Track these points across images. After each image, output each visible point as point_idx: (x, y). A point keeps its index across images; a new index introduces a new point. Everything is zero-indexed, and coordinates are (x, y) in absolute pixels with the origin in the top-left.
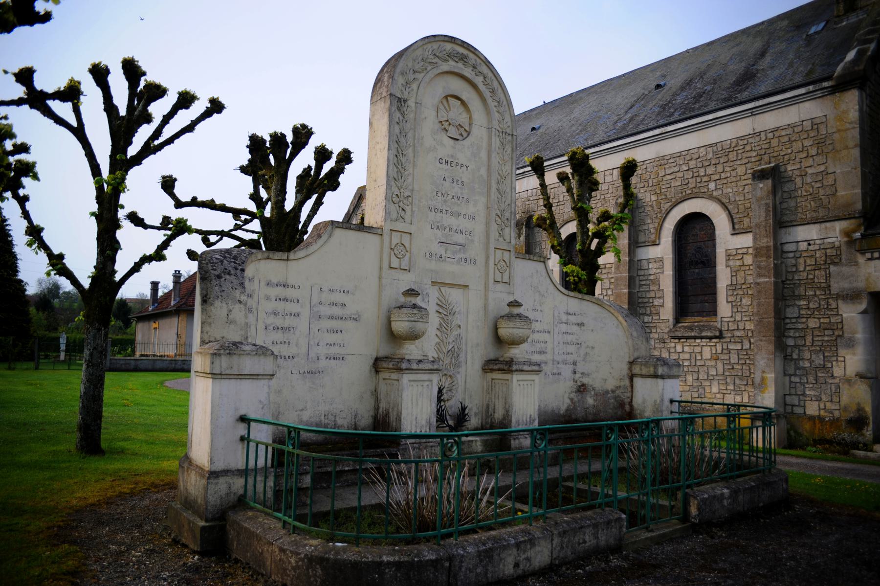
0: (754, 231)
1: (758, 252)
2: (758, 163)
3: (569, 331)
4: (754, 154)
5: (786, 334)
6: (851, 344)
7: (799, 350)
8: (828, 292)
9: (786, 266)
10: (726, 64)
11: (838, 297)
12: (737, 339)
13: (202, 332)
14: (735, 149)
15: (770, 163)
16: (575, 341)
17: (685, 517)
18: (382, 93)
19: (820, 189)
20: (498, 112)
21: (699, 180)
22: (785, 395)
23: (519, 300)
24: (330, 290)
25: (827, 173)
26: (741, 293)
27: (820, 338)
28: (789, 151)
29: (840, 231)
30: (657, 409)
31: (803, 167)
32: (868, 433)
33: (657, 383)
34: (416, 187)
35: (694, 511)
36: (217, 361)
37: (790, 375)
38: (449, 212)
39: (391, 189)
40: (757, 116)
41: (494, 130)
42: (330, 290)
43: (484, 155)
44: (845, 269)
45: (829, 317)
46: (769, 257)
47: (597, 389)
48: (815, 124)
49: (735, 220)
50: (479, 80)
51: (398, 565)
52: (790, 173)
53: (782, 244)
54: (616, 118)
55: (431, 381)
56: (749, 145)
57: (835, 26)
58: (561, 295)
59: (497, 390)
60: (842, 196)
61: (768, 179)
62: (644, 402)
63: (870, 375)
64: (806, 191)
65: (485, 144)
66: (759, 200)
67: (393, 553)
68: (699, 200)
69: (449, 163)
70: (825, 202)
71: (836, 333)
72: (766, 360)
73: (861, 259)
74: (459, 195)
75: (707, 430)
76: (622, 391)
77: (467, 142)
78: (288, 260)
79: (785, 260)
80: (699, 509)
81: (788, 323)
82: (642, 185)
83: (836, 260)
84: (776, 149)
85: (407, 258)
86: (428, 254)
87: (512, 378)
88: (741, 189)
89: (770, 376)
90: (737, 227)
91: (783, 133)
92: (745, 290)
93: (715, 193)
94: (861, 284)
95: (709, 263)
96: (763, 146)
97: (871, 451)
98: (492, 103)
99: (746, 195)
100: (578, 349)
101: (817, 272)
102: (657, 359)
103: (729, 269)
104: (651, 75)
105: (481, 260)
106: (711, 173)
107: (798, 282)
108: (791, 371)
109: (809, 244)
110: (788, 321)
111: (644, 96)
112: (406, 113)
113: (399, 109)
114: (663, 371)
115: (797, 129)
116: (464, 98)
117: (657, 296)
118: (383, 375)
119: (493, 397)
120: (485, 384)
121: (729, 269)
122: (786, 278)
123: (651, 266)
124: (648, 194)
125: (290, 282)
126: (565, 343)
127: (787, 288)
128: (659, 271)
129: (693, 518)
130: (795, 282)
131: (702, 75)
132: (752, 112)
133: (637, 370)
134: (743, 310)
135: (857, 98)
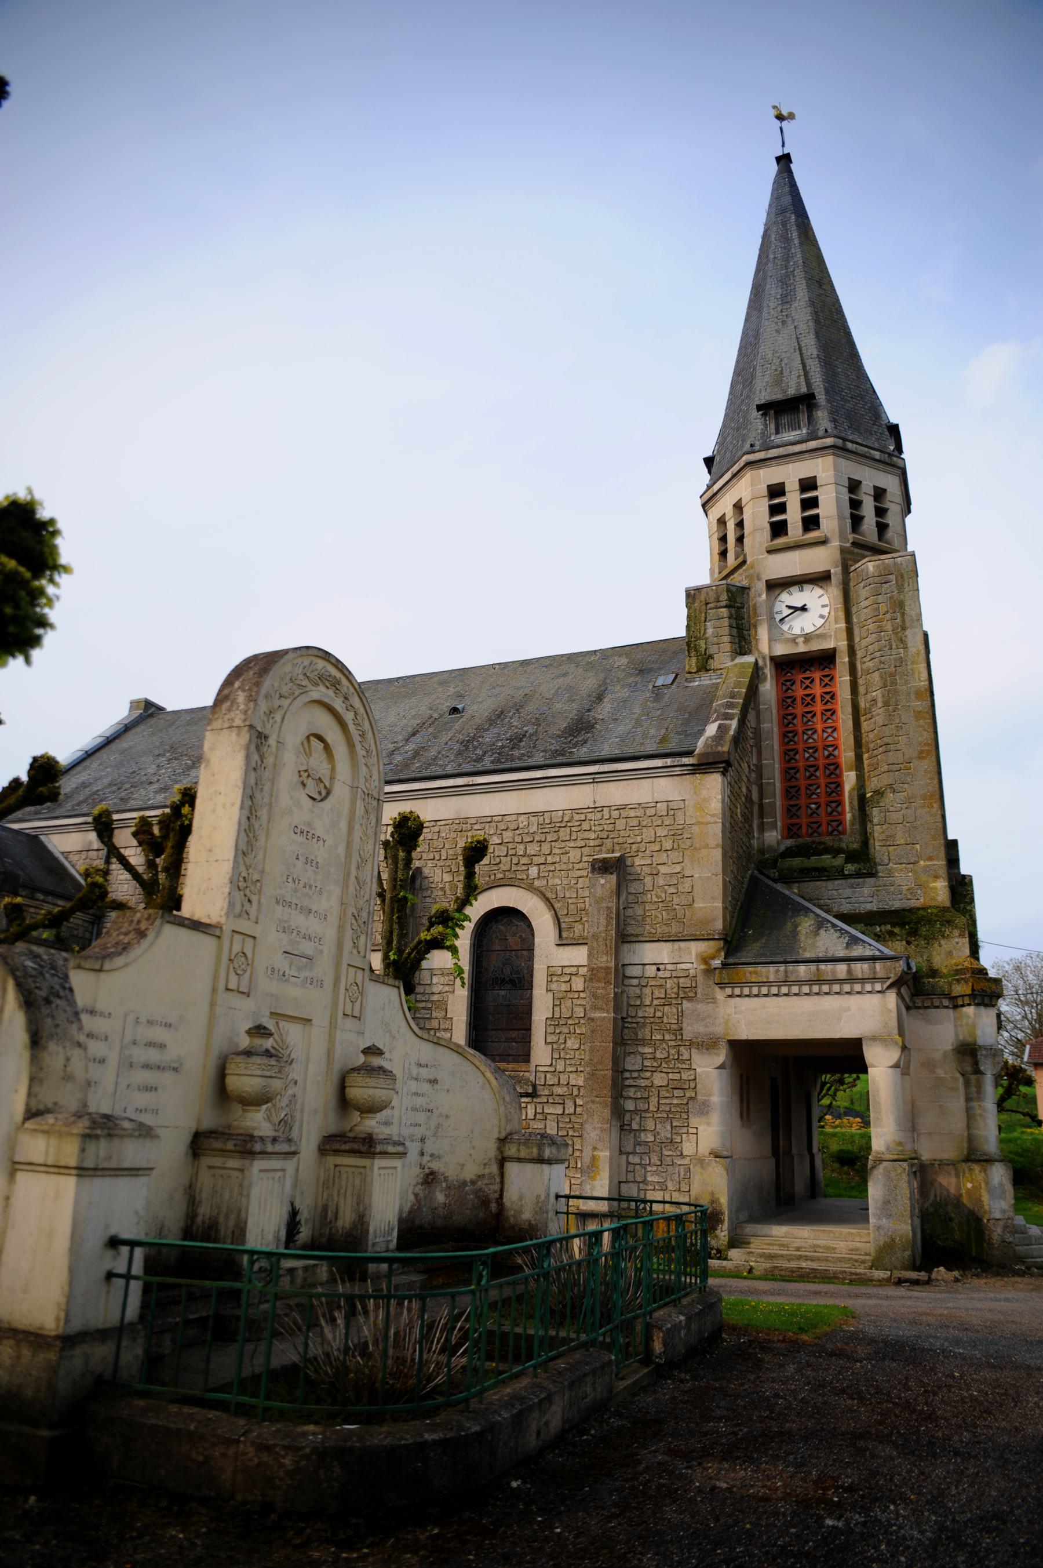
0: (589, 942)
1: (594, 974)
2: (597, 849)
3: (419, 1092)
4: (593, 836)
5: (624, 1093)
6: (704, 1110)
7: (641, 1117)
8: (679, 1037)
9: (628, 997)
10: (551, 699)
11: (692, 1044)
12: (557, 1098)
13: (29, 1095)
14: (569, 824)
15: (613, 852)
16: (425, 1106)
17: (647, 1359)
18: (233, 720)
19: (674, 896)
20: (366, 765)
21: (515, 860)
22: (620, 1182)
23: (381, 1046)
24: (148, 1022)
25: (684, 876)
26: (566, 1031)
27: (667, 1101)
28: (639, 839)
29: (697, 955)
30: (540, 1208)
31: (655, 863)
32: (723, 1234)
33: (542, 1170)
34: (267, 869)
35: (658, 1347)
36: (91, 1148)
37: (628, 1154)
38: (299, 906)
39: (238, 868)
40: (600, 785)
41: (359, 790)
42: (148, 1022)
43: (343, 825)
44: (701, 1007)
45: (679, 1072)
46: (608, 983)
47: (450, 1179)
48: (672, 810)
49: (563, 925)
50: (348, 717)
51: (443, 1443)
52: (639, 868)
53: (623, 965)
54: (391, 746)
55: (284, 1170)
56: (587, 821)
57: (686, 684)
58: (413, 1037)
59: (344, 1182)
60: (701, 909)
61: (611, 873)
62: (521, 1199)
63: (725, 1153)
64: (657, 897)
65: (346, 811)
66: (598, 901)
67: (432, 1428)
68: (515, 888)
69: (305, 833)
70: (680, 914)
71: (688, 1095)
72: (598, 1132)
73: (720, 995)
74: (312, 882)
75: (555, 1237)
76: (486, 1182)
77: (326, 805)
78: (100, 970)
79: (626, 989)
80: (665, 1344)
81: (627, 1078)
82: (431, 856)
83: (691, 994)
84: (622, 833)
85: (247, 975)
86: (269, 969)
87: (373, 1164)
88: (573, 882)
89: (604, 1155)
90: (564, 935)
91: (632, 813)
92: (572, 1027)
93: (537, 883)
94: (718, 1029)
95: (522, 982)
96: (605, 826)
97: (726, 1259)
98: (361, 752)
99: (580, 890)
100: (429, 1118)
101: (666, 1008)
102: (542, 1135)
103: (550, 995)
104: (440, 690)
105: (329, 983)
106: (533, 853)
107: (642, 1020)
108: (630, 1149)
109: (658, 969)
110: (627, 1075)
111: (431, 721)
112: (266, 756)
113: (258, 748)
114: (551, 1153)
115: (651, 812)
116: (329, 740)
117: (442, 1027)
118: (206, 1161)
119: (335, 1194)
120: (322, 1173)
121: (550, 995)
122: (627, 1014)
123: (435, 980)
124: (438, 871)
125: (100, 1006)
126: (414, 1109)
127: (627, 1028)
128: (447, 988)
129: (657, 1357)
130: (639, 1020)
131: (518, 707)
132: (595, 779)
133: (511, 1150)
134: (568, 1056)
135: (719, 786)
